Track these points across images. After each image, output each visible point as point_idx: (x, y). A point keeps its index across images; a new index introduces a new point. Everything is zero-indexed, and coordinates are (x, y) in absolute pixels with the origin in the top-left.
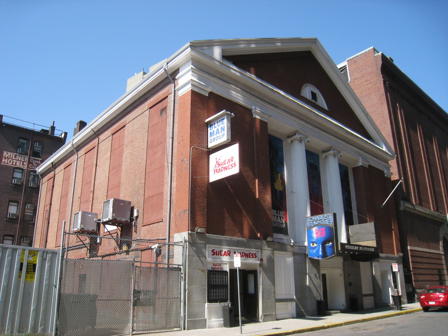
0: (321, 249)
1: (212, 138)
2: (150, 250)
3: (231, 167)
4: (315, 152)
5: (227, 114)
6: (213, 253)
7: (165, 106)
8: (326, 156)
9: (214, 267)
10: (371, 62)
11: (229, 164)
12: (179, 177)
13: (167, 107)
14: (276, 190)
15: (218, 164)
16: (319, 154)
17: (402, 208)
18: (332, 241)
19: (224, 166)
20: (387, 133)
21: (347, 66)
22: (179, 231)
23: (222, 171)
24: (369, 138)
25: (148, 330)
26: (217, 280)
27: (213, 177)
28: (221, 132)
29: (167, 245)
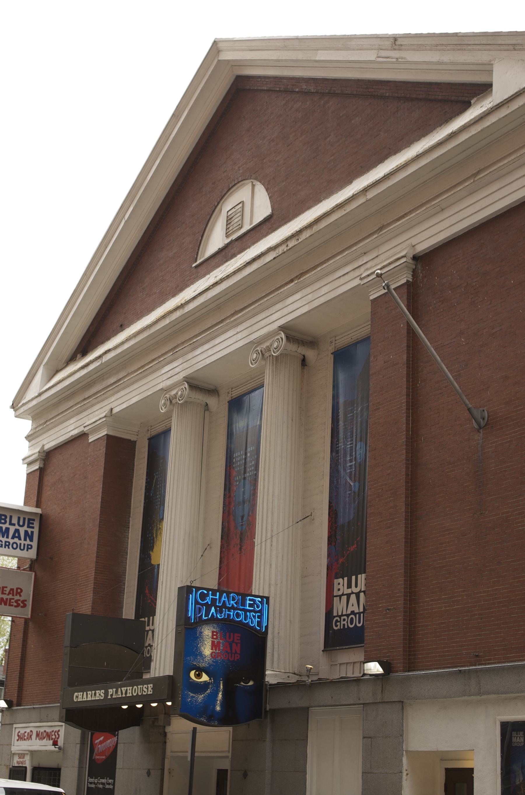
0: (220, 696)
6: (25, 602)
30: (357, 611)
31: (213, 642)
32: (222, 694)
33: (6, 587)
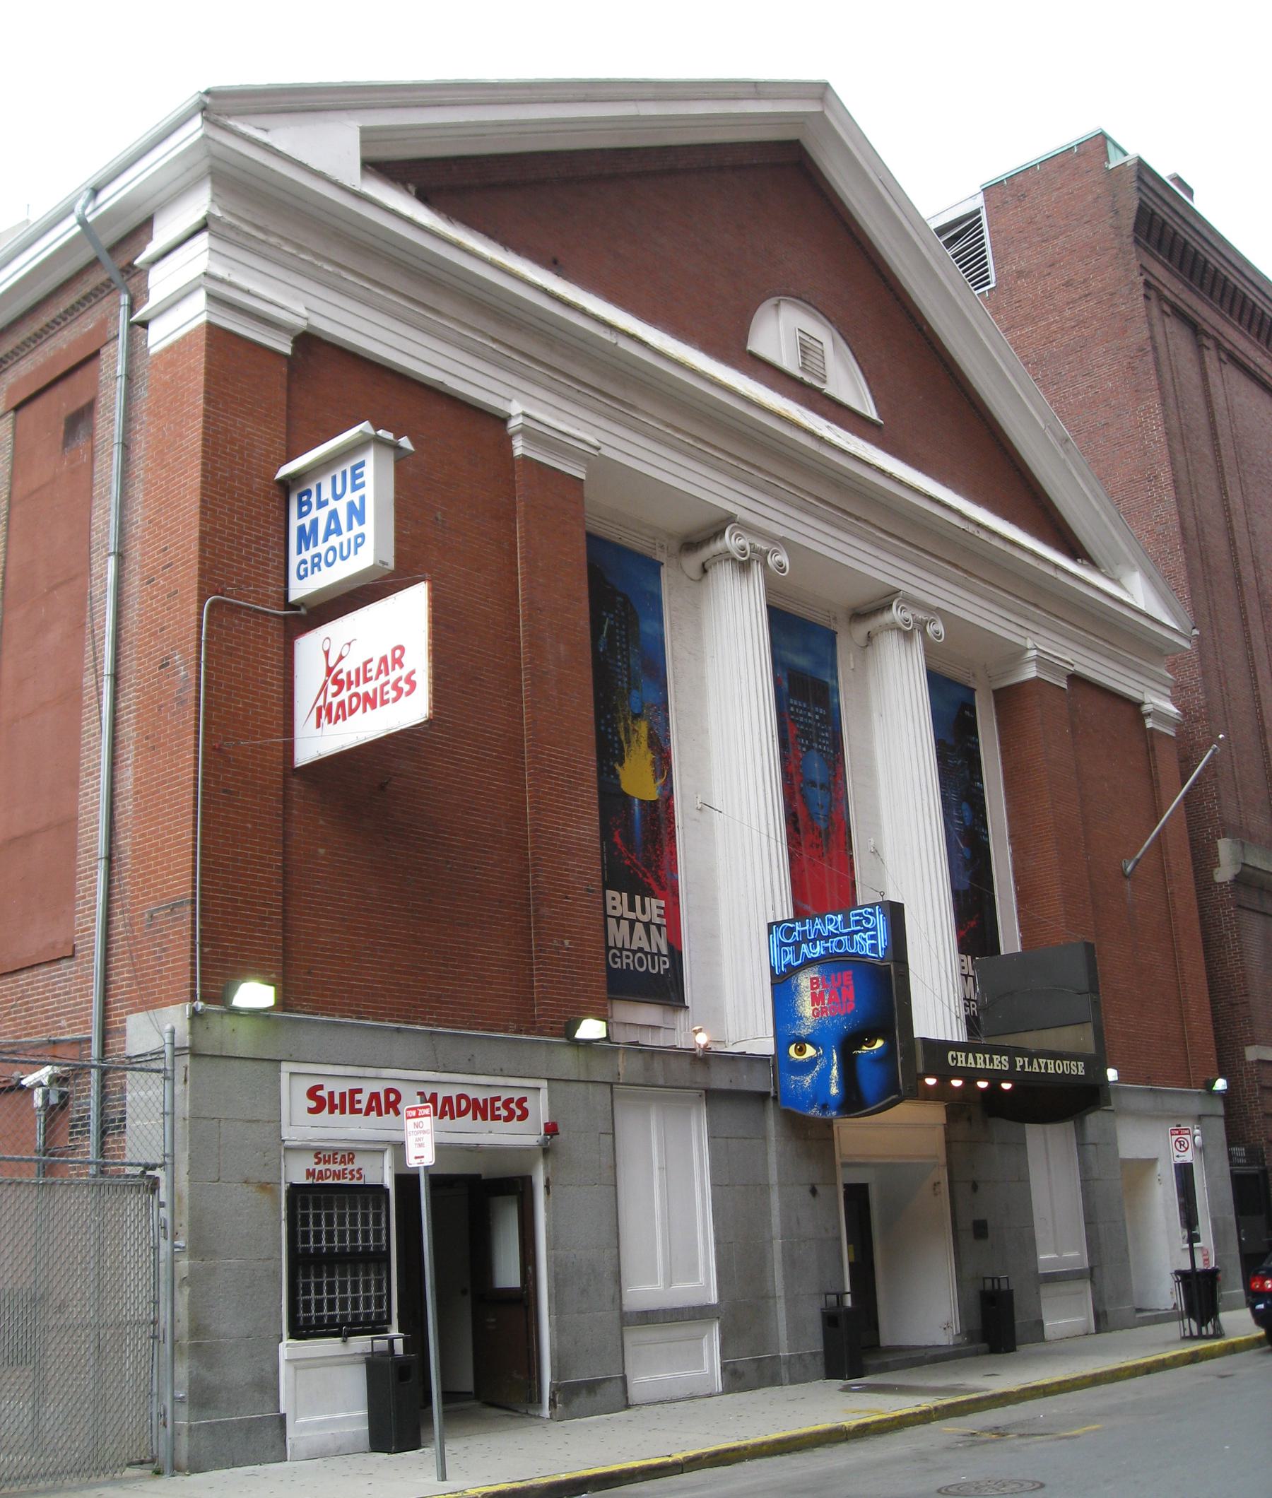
0: (835, 1072)
1: (306, 555)
2: (19, 1095)
3: (393, 694)
4: (819, 618)
5: (379, 441)
6: (313, 1104)
7: (83, 402)
8: (870, 637)
9: (321, 1167)
10: (1090, 198)
11: (383, 678)
12: (151, 744)
13: (99, 406)
14: (627, 798)
15: (335, 682)
16: (834, 627)
17: (1225, 873)
18: (887, 1034)
19: (363, 689)
20: (1160, 528)
21: (983, 214)
22: (148, 1003)
23: (352, 712)
24: (1075, 550)
25: (98, 1465)
26: (341, 1232)
27: (315, 742)
28: (350, 528)
29: (94, 1072)
30: (647, 949)
31: (813, 995)
32: (838, 1070)
33: (371, 660)
